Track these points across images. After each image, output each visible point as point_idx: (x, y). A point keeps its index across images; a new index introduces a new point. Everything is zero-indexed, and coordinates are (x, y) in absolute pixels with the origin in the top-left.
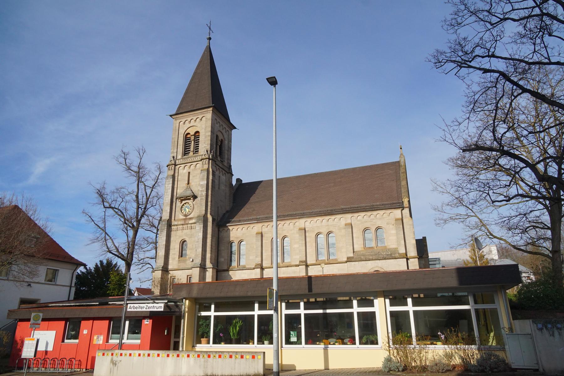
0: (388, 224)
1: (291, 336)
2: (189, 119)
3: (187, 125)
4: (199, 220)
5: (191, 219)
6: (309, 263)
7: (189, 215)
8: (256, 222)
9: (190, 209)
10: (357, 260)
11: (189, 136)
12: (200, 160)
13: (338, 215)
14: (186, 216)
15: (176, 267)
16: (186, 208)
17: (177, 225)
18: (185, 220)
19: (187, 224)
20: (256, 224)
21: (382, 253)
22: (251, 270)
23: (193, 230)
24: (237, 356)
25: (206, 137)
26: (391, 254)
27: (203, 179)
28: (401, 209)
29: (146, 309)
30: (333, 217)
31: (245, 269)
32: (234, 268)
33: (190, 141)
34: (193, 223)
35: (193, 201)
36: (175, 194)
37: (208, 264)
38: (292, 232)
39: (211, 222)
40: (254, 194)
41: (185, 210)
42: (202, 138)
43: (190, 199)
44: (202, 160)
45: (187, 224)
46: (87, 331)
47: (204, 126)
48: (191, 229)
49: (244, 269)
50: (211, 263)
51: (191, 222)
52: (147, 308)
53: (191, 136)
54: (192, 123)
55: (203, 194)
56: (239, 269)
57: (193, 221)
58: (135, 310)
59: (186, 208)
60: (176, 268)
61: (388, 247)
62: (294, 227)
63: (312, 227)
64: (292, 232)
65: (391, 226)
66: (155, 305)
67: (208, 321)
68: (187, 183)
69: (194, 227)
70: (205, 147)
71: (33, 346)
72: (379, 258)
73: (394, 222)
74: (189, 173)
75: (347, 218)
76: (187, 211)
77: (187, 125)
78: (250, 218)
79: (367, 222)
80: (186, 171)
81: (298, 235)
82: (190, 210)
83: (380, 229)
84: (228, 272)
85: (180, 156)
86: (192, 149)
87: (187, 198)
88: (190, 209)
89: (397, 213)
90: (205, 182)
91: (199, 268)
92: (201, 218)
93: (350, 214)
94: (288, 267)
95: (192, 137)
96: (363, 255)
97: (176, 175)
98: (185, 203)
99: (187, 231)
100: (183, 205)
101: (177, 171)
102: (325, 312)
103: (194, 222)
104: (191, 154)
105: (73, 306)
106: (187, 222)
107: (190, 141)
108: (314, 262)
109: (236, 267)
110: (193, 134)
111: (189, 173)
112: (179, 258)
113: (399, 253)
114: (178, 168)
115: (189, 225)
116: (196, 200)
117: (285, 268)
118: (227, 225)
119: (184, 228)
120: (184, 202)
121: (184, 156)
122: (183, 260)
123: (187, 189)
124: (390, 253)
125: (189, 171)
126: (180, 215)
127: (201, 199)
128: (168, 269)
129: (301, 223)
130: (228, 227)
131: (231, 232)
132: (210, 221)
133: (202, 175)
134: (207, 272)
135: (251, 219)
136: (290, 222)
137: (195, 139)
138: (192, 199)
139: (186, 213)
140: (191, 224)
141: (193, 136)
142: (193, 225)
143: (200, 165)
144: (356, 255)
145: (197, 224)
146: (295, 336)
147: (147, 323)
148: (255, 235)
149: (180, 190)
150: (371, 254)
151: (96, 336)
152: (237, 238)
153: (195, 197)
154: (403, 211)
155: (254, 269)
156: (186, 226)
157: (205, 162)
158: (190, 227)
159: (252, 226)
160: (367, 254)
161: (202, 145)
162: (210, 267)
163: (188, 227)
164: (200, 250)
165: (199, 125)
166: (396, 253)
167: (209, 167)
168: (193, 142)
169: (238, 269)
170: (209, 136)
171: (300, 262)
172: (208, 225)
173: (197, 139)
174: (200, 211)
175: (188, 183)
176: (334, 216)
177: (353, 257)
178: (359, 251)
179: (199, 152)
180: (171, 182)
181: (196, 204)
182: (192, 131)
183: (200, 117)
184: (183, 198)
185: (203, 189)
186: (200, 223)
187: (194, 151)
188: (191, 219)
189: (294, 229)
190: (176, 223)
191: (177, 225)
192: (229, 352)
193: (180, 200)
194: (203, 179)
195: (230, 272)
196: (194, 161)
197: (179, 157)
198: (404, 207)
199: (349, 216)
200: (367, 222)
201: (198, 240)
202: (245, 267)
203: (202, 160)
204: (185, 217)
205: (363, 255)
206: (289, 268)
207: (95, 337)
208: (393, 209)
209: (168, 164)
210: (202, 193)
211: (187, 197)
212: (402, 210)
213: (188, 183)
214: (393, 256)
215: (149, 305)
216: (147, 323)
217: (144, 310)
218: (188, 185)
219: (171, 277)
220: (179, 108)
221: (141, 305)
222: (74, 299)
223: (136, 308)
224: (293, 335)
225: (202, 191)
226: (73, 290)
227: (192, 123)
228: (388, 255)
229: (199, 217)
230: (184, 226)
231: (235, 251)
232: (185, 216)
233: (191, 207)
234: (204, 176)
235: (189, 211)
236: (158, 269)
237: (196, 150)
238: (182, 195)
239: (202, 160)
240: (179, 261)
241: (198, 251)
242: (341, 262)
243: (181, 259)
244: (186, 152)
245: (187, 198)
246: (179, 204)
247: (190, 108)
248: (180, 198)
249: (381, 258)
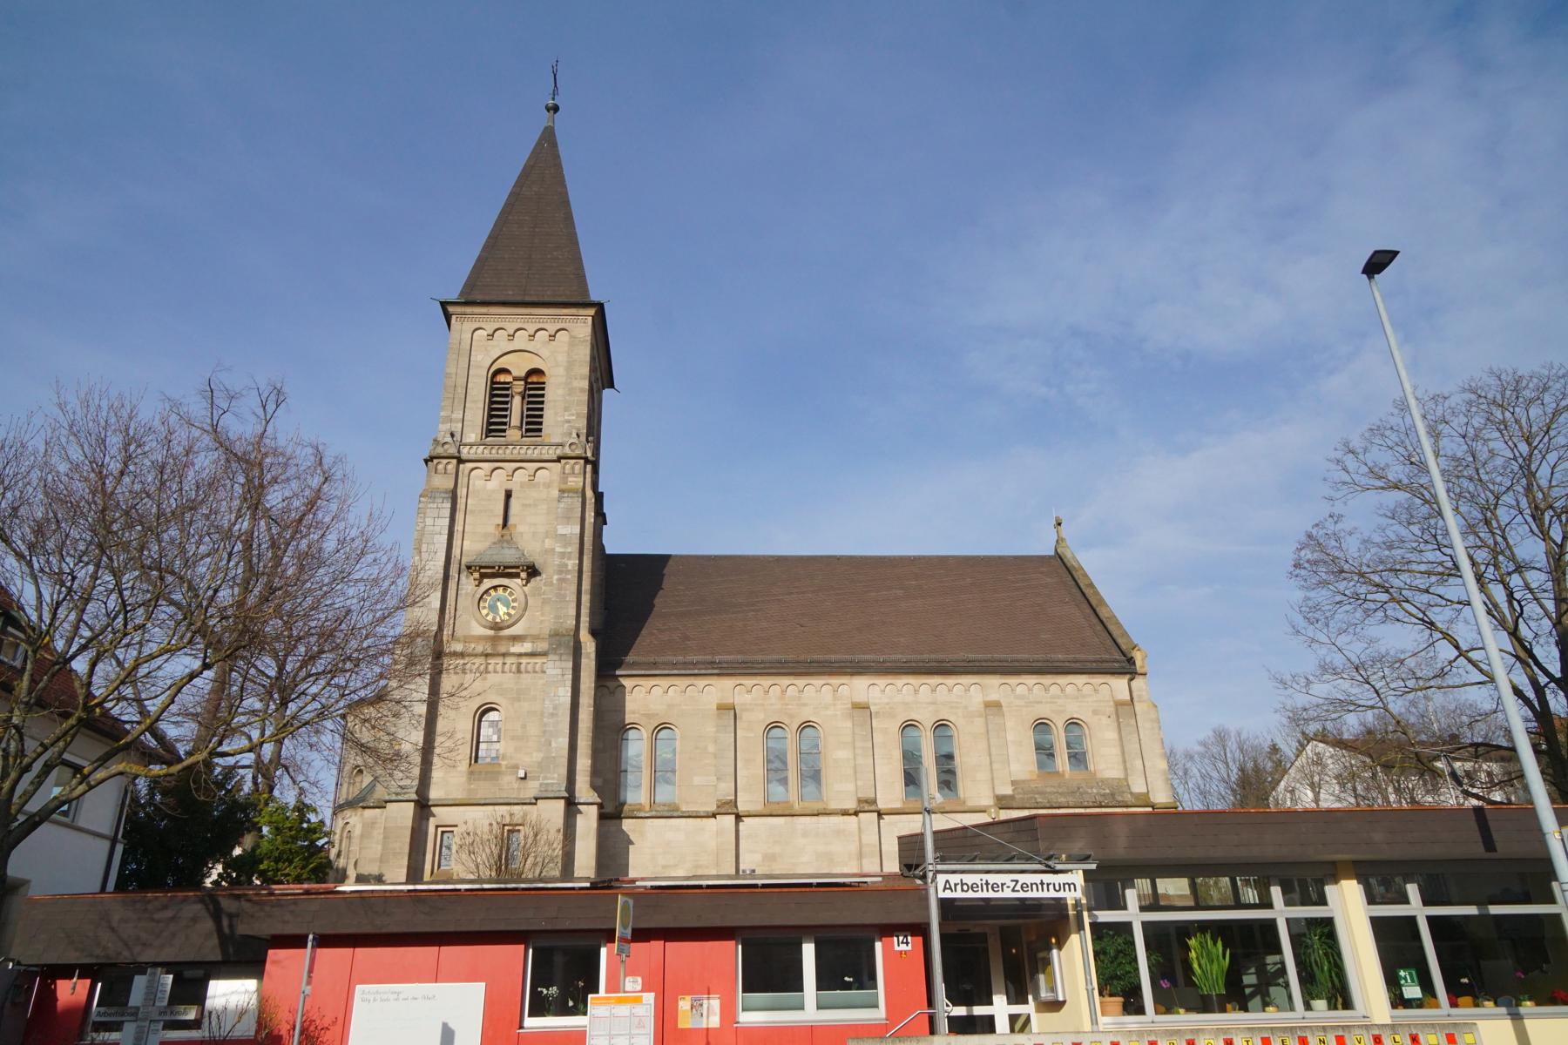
0: (1095, 712)
1: (1403, 982)
2: (511, 327)
3: (501, 343)
4: (559, 645)
5: (515, 639)
6: (742, 808)
7: (509, 627)
8: (943, 665)
9: (513, 608)
10: (1028, 806)
11: (502, 378)
12: (555, 458)
13: (963, 676)
14: (497, 627)
15: (458, 795)
16: (499, 604)
17: (462, 655)
18: (494, 640)
19: (504, 655)
20: (716, 677)
21: (1090, 791)
22: (699, 820)
23: (524, 676)
24: (1398, 1038)
25: (571, 391)
26: (1113, 795)
27: (569, 518)
28: (1128, 676)
29: (1013, 890)
30: (950, 681)
31: (679, 814)
32: (639, 810)
33: (507, 396)
34: (526, 655)
35: (526, 585)
36: (456, 551)
37: (584, 791)
38: (829, 713)
39: (593, 656)
40: (661, 591)
41: (493, 608)
42: (555, 395)
43: (517, 576)
44: (559, 460)
45: (504, 655)
46: (639, 979)
47: (562, 358)
48: (519, 671)
49: (675, 814)
50: (594, 787)
51: (516, 649)
52: (1018, 887)
53: (515, 379)
54: (521, 341)
55: (567, 565)
56: (659, 814)
57: (527, 647)
58: (971, 894)
59: (499, 604)
60: (460, 797)
61: (1099, 775)
62: (835, 698)
63: (888, 704)
64: (829, 713)
65: (1105, 720)
66: (1048, 878)
67: (1098, 948)
68: (500, 521)
69: (530, 667)
70: (569, 422)
71: (641, 1025)
72: (1086, 804)
73: (1111, 709)
74: (508, 495)
75: (993, 687)
76: (501, 613)
77: (501, 343)
78: (689, 658)
79: (1041, 702)
80: (498, 483)
81: (849, 724)
82: (513, 612)
83: (1075, 726)
84: (617, 821)
85: (473, 436)
86: (515, 420)
87: (507, 571)
88: (513, 608)
89: (1119, 685)
90: (577, 530)
91: (413, 804)
92: (563, 639)
93: (998, 676)
94: (817, 815)
95: (515, 383)
96: (1039, 793)
97: (462, 492)
98: (495, 588)
99: (508, 680)
100: (486, 592)
101: (462, 480)
102: (1484, 912)
103: (529, 651)
104: (513, 434)
105: (524, 889)
106: (502, 649)
107: (507, 396)
108: (759, 807)
109: (647, 808)
110: (523, 374)
111: (508, 495)
112: (470, 764)
113: (1131, 793)
114: (467, 472)
115: (509, 660)
116: (535, 581)
117: (808, 818)
118: (618, 673)
119: (523, 667)
120: (488, 583)
121: (487, 437)
122: (487, 772)
123: (500, 541)
124: (1108, 791)
125: (509, 487)
126: (474, 624)
127: (559, 580)
128: (428, 800)
129: (861, 687)
130: (621, 679)
131: (628, 697)
132: (589, 658)
133: (562, 505)
134: (578, 816)
135: (692, 664)
136: (771, 682)
137: (525, 390)
138: (523, 575)
139: (498, 620)
140: (520, 655)
141: (522, 383)
142: (524, 660)
143: (551, 473)
144: (1020, 790)
145: (551, 657)
146: (1413, 981)
147: (903, 947)
148: (716, 712)
149: (477, 540)
150: (1060, 791)
151: (688, 998)
152: (649, 716)
153: (533, 572)
154: (1134, 683)
155: (714, 816)
156: (500, 660)
157: (573, 468)
158: (514, 667)
159: (701, 682)
160: (1048, 790)
161: (556, 414)
162: (591, 801)
163: (504, 664)
164: (563, 742)
165: (544, 352)
166: (1123, 792)
167: (584, 483)
168: (517, 400)
169: (654, 813)
170: (582, 390)
171: (860, 801)
172: (582, 666)
173: (531, 392)
174: (558, 617)
175: (505, 524)
176: (954, 677)
177: (1012, 797)
178: (1024, 781)
179: (542, 434)
180: (447, 513)
181: (534, 595)
182: (519, 366)
183: (552, 328)
184: (494, 568)
185: (569, 550)
186: (561, 654)
187: (521, 427)
188: (515, 639)
189: (835, 705)
190: (458, 647)
191: (462, 655)
192: (1261, 1029)
193: (477, 575)
194: (567, 519)
195: (624, 820)
196: (528, 457)
197: (472, 435)
198: (1136, 673)
199: (993, 681)
200: (1041, 702)
201: (555, 708)
202: (677, 810)
203: (559, 460)
204: (491, 633)
205: (1039, 793)
206: (822, 819)
207: (684, 1004)
208: (1108, 676)
209: (426, 456)
210: (566, 561)
211: (505, 567)
212: (1131, 680)
213: (505, 524)
214: (1120, 799)
215: (1023, 878)
216: (903, 947)
217: (1008, 894)
218: (505, 531)
219: (437, 827)
220: (471, 284)
221: (992, 878)
222: (115, 889)
223: (973, 887)
224: (1405, 979)
225: (563, 555)
226: (119, 848)
227: (521, 341)
228: (1104, 795)
229: (555, 635)
230: (492, 661)
231: (638, 756)
232: (491, 629)
233: (514, 601)
234: (570, 509)
235: (509, 614)
236: (400, 798)
237: (533, 424)
238: (486, 560)
239: (563, 461)
240: (471, 773)
241: (553, 745)
242: (978, 809)
243: (475, 767)
244: (494, 424)
245: (507, 571)
246: (468, 583)
247: (510, 295)
248: (481, 567)
249: (1091, 804)
